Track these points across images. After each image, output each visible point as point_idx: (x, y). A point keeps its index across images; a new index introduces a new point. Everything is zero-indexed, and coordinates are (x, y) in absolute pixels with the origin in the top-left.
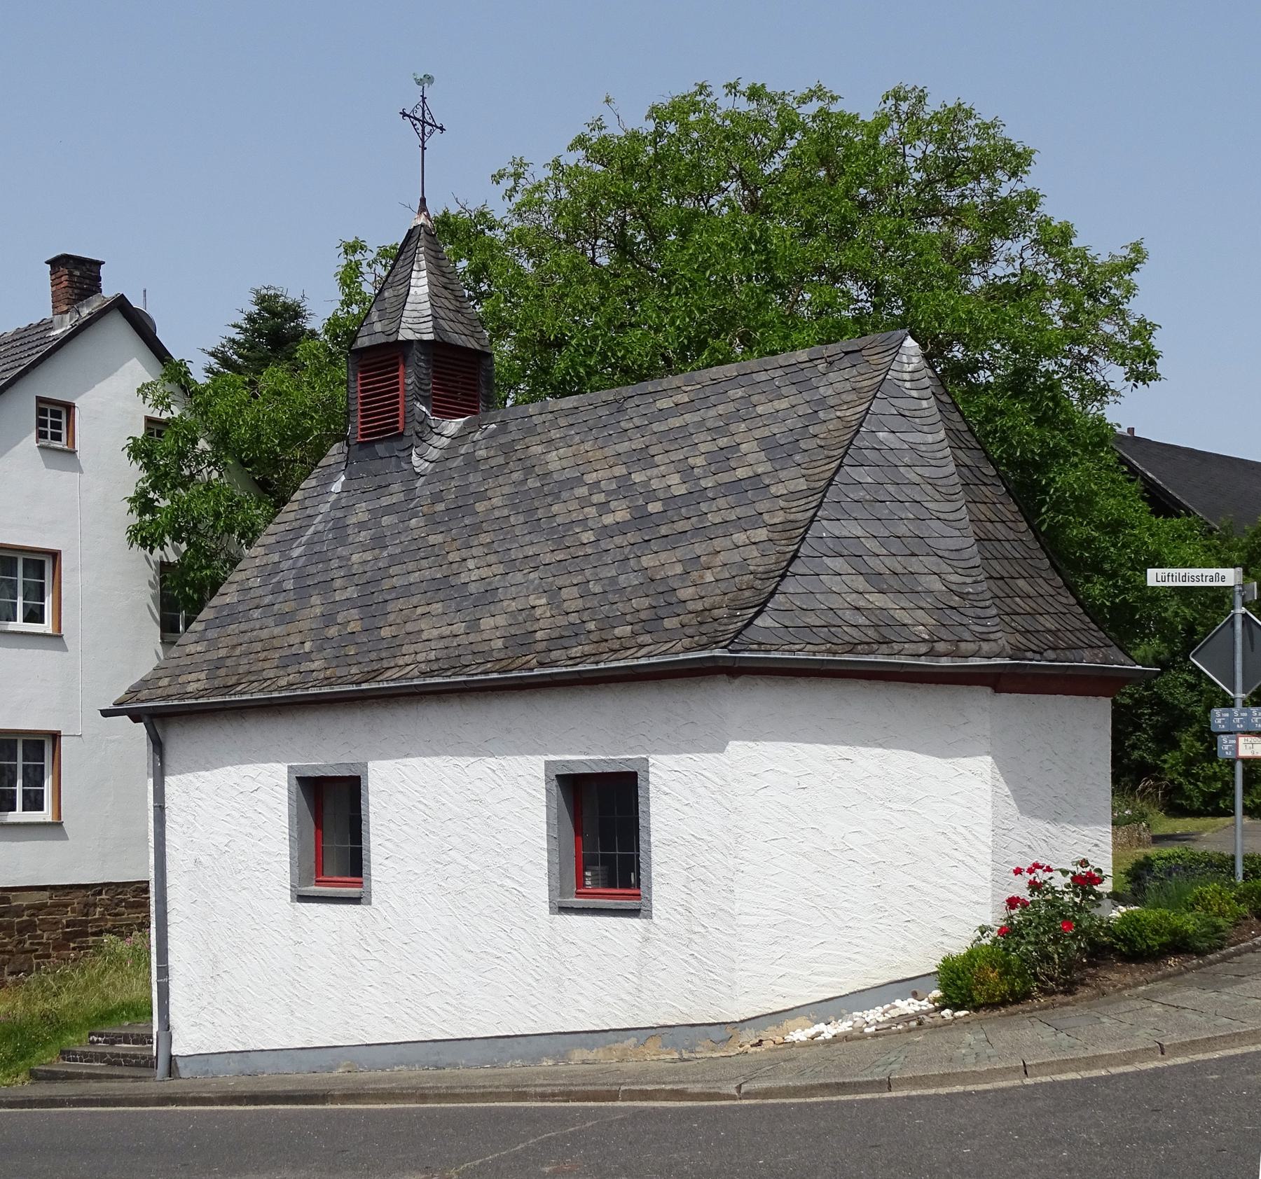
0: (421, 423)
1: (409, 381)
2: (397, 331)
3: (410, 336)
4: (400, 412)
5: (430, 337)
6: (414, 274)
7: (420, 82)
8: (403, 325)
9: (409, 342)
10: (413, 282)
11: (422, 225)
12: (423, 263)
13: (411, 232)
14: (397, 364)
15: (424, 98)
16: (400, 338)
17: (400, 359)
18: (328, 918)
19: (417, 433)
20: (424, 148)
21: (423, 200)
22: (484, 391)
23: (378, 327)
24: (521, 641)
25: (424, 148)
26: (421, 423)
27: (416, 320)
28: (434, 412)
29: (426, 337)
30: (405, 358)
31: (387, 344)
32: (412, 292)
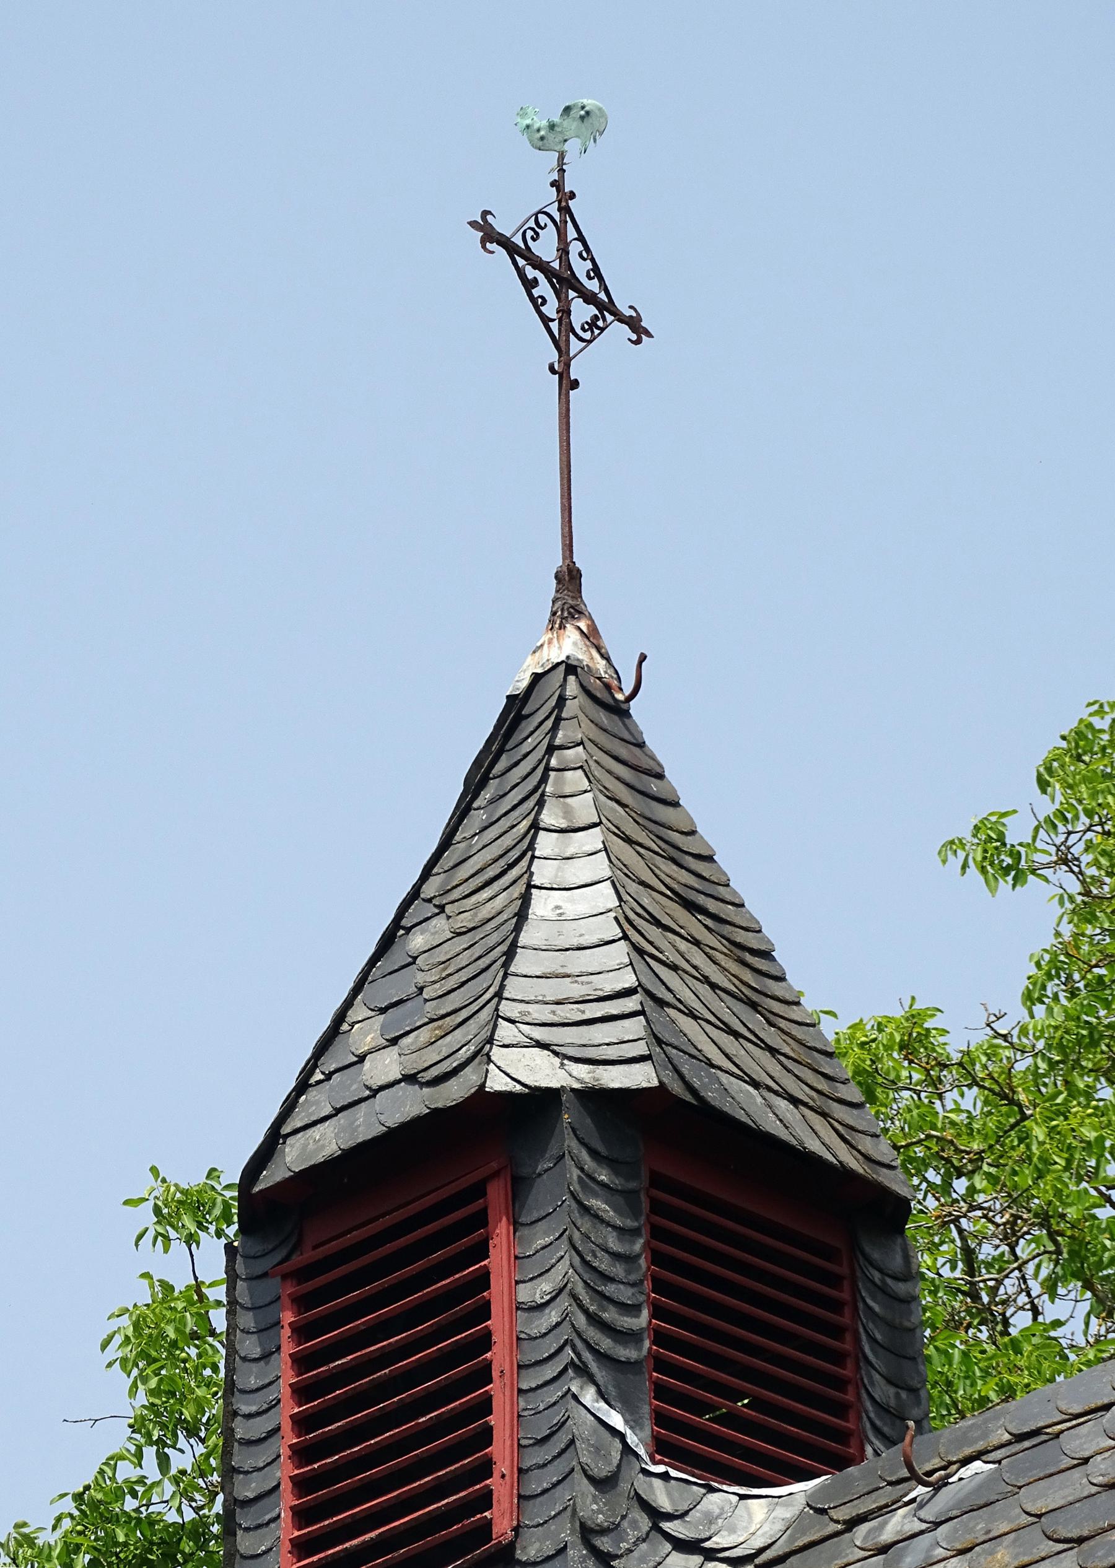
0: (604, 1484)
1: (544, 1288)
2: (481, 1055)
3: (541, 1071)
4: (501, 1450)
5: (641, 1077)
6: (546, 843)
7: (544, 139)
8: (506, 1032)
9: (542, 1101)
10: (542, 873)
11: (570, 668)
12: (584, 808)
13: (516, 710)
14: (481, 1220)
15: (565, 199)
16: (497, 1083)
17: (497, 1193)
18: (646, 653)
19: (587, 1533)
20: (568, 384)
21: (569, 579)
22: (883, 1391)
23: (385, 1066)
24: (992, 1553)
25: (568, 384)
26: (604, 1484)
27: (572, 1013)
28: (662, 1448)
29: (616, 1078)
30: (520, 1187)
31: (435, 1120)
32: (542, 905)
